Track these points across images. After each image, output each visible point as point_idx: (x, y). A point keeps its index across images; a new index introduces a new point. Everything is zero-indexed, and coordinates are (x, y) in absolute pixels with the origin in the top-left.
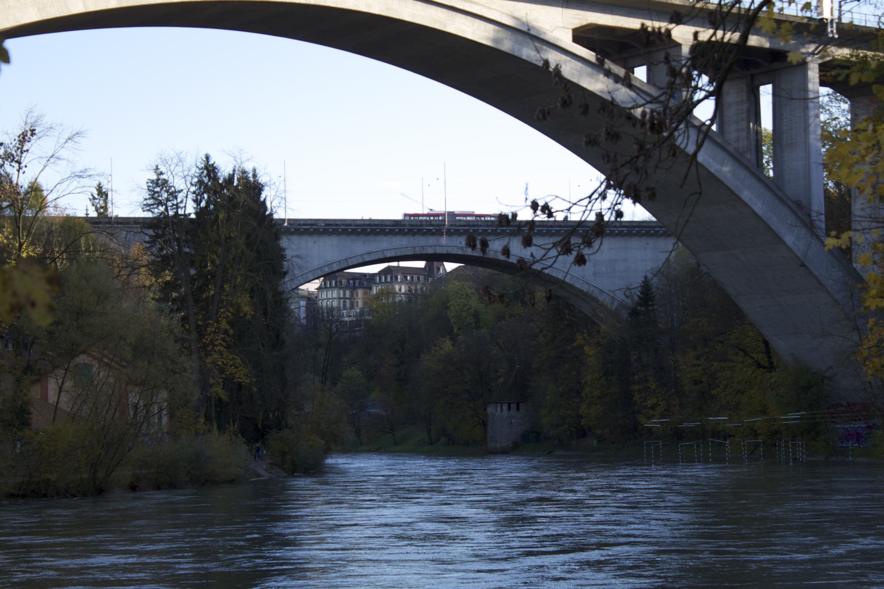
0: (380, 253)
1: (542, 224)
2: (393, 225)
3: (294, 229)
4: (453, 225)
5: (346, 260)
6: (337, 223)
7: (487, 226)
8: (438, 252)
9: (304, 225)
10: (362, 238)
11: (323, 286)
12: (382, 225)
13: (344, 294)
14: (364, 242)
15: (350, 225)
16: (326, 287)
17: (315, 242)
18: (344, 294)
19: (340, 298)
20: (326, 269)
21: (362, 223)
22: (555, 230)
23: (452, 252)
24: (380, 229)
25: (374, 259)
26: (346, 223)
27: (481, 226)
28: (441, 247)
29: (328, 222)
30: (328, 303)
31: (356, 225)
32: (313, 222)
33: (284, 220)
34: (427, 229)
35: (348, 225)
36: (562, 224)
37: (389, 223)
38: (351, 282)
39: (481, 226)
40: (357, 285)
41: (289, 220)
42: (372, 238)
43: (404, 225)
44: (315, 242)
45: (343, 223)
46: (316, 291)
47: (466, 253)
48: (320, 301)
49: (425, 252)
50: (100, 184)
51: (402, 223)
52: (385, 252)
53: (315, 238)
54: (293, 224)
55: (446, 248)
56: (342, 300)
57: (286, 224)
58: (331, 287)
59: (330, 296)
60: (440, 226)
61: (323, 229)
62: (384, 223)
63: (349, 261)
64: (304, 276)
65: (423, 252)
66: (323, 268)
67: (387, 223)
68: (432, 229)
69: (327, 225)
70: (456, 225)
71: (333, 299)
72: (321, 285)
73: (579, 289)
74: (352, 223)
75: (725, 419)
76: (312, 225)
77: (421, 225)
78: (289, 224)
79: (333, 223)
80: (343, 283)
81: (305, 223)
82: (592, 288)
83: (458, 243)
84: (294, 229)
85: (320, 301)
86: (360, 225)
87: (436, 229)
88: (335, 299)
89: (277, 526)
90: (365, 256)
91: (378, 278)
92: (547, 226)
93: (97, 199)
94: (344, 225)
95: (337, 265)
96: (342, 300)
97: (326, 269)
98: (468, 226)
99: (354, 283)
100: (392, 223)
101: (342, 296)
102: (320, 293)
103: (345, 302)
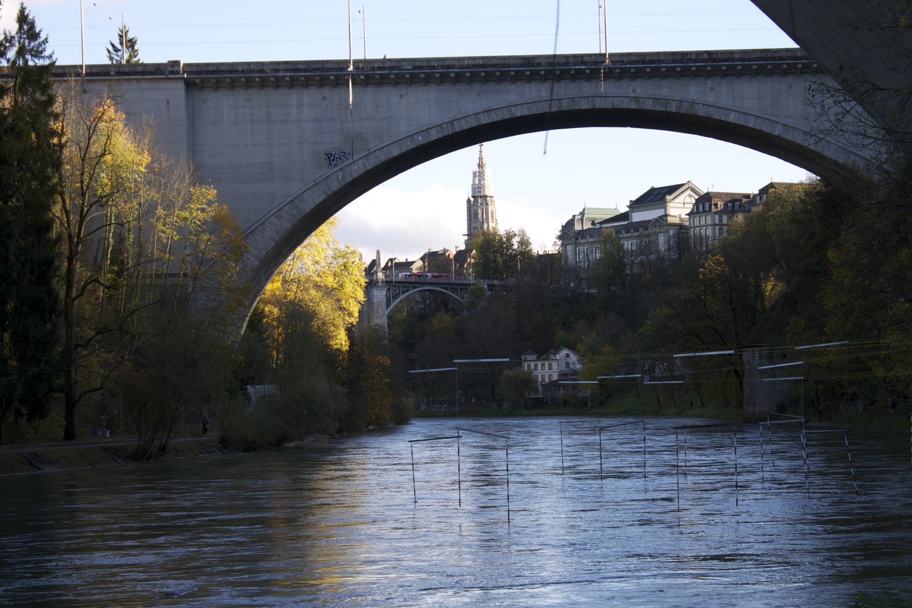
0: (505, 110)
1: (764, 54)
2: (522, 65)
3: (365, 75)
4: (618, 62)
5: (451, 122)
6: (432, 64)
7: (674, 61)
8: (597, 107)
9: (380, 68)
10: (477, 87)
11: (695, 211)
12: (503, 66)
13: (721, 220)
14: (479, 94)
15: (453, 67)
16: (698, 212)
17: (402, 97)
18: (721, 220)
19: (715, 225)
20: (420, 138)
21: (471, 63)
22: (787, 64)
23: (621, 106)
24: (500, 72)
25: (495, 120)
26: (446, 63)
27: (663, 62)
28: (603, 99)
29: (417, 64)
30: (702, 231)
31: (462, 67)
32: (394, 64)
33: (347, 62)
34: (576, 70)
35: (449, 67)
36: (799, 54)
37: (514, 61)
38: (729, 204)
39: (663, 62)
40: (737, 208)
41: (356, 62)
42: (491, 87)
43: (539, 64)
44: (402, 97)
45: (441, 63)
46: (687, 217)
47: (644, 107)
48: (692, 229)
49: (577, 107)
50: (22, 10)
51: (536, 61)
52: (513, 108)
53: (402, 90)
54: (363, 68)
55: (611, 99)
56: (717, 228)
57: (351, 68)
58: (704, 211)
59: (703, 223)
60: (596, 63)
61: (410, 74)
62: (507, 62)
63: (456, 124)
64: (386, 150)
65: (574, 108)
66: (415, 137)
67: (512, 62)
68: (584, 70)
69: (415, 68)
70: (622, 61)
71: (707, 226)
72: (693, 209)
73: (830, 160)
74: (456, 63)
75: (730, 355)
76: (392, 68)
77: (566, 64)
78: (355, 68)
79: (425, 64)
80: (719, 206)
81: (381, 65)
82: (852, 158)
83: (631, 90)
84: (365, 75)
85: (692, 229)
86: (468, 66)
87: (591, 69)
88: (709, 225)
89: (300, 537)
90: (482, 115)
91: (758, 198)
92: (773, 59)
93: (120, 50)
94: (442, 67)
95: (438, 131)
96: (717, 228)
97: (420, 138)
98: (643, 62)
99: (733, 206)
100: (520, 61)
101: (717, 222)
102: (692, 218)
103: (720, 229)
